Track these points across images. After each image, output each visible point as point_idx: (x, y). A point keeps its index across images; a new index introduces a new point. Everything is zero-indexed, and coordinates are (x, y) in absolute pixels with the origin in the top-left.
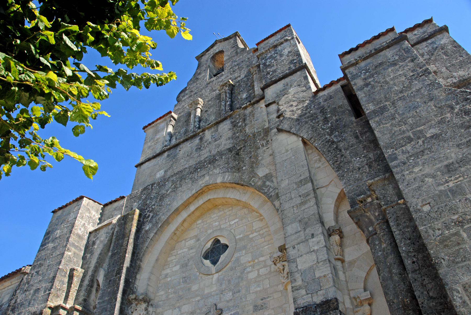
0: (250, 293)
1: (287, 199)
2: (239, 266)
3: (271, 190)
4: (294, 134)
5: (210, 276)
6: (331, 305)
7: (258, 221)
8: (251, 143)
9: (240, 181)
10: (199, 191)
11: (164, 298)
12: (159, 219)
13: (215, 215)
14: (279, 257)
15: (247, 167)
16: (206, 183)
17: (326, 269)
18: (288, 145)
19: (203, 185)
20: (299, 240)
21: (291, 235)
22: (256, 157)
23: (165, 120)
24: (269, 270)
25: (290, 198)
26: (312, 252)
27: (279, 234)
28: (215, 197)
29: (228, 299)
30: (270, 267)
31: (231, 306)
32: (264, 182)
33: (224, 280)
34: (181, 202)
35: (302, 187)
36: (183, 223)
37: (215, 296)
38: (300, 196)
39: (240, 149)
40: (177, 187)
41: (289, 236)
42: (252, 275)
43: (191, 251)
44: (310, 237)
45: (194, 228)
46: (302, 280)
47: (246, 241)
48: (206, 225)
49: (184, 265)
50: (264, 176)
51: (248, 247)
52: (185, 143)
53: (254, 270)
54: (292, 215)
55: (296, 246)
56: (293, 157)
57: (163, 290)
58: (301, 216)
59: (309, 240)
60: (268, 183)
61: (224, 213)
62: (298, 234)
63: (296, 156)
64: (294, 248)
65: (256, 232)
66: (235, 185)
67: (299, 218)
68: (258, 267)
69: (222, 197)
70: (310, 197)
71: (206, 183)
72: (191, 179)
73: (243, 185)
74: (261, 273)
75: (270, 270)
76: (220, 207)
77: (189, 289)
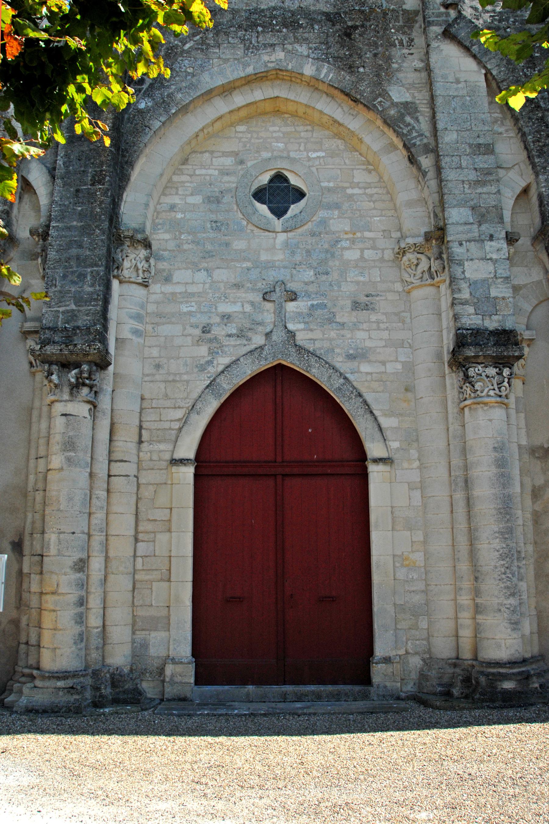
0: (346, 281)
1: (454, 165)
2: (326, 233)
3: (415, 134)
4: (474, 57)
5: (271, 234)
6: (511, 337)
7: (364, 170)
8: (377, 26)
9: (353, 91)
10: (262, 72)
11: (171, 245)
12: (169, 96)
13: (277, 128)
14: (415, 244)
15: (367, 70)
16: (277, 64)
17: (506, 290)
18: (460, 71)
19: (271, 65)
20: (470, 236)
21: (458, 224)
22: (389, 59)
24: (380, 255)
25: (459, 165)
26: (488, 259)
27: (415, 210)
28: (291, 96)
29: (306, 280)
30: (383, 252)
31: (311, 292)
32: (402, 116)
33: (298, 248)
34: (219, 81)
35: (480, 157)
36: (216, 121)
37: (282, 270)
38: (476, 169)
39: (355, 27)
40: (209, 44)
41: (453, 224)
42: (352, 255)
43: (226, 178)
44: (488, 238)
45: (230, 138)
46: (471, 294)
47: (339, 196)
48: (257, 141)
49: (212, 199)
50: (402, 104)
51: (344, 208)
53: (354, 247)
54: (461, 194)
55: (464, 243)
56: (468, 98)
57: (166, 232)
58: (475, 201)
59: (485, 242)
60: (408, 119)
61: (296, 131)
62: (469, 227)
63: (473, 98)
64: (461, 244)
65: (360, 188)
66: (336, 92)
67: (472, 203)
68: (361, 245)
69: (305, 103)
70: (491, 178)
71: (277, 64)
72: (243, 40)
73: (356, 101)
74: (366, 256)
75: (383, 257)
76: (286, 116)
77: (227, 244)
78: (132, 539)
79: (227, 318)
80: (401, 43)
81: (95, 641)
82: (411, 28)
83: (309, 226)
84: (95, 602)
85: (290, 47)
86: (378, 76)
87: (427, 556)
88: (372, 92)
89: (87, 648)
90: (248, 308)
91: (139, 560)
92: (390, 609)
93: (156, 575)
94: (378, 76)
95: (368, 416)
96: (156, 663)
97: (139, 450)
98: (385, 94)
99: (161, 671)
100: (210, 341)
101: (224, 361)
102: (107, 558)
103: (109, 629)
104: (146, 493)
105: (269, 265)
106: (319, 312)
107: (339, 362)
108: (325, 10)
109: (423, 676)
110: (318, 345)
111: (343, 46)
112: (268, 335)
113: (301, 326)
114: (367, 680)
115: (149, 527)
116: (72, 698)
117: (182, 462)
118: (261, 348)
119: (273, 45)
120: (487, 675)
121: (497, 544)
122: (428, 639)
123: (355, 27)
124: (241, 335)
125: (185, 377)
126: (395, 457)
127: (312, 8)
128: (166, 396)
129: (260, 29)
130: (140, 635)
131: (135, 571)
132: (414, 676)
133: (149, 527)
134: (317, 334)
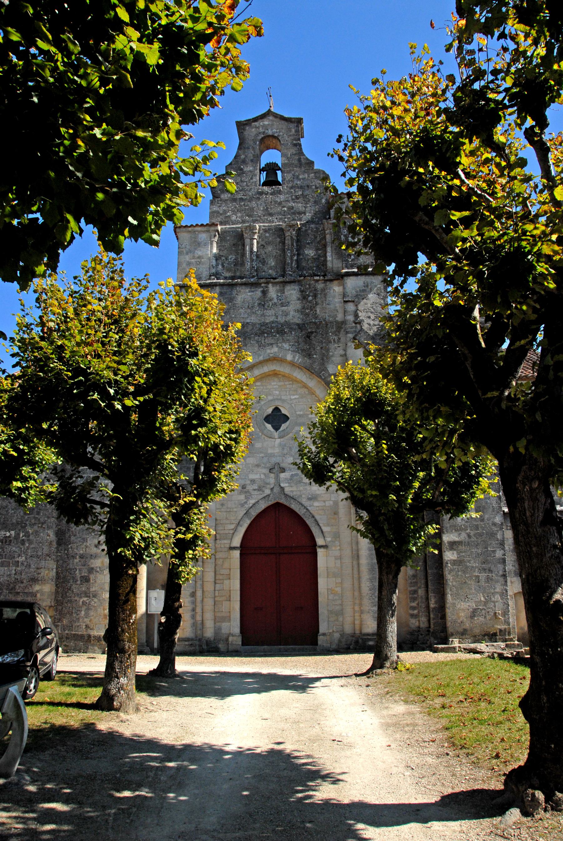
13: (275, 383)
19: (271, 355)
22: (328, 350)
23: (208, 231)
52: (244, 287)
72: (258, 342)
78: (213, 583)
79: (253, 481)
80: (334, 341)
81: (199, 626)
82: (339, 332)
83: (291, 435)
84: (199, 610)
85: (280, 345)
86: (323, 359)
87: (342, 589)
88: (320, 368)
89: (196, 629)
90: (263, 476)
91: (217, 592)
92: (326, 612)
93: (224, 598)
94: (323, 359)
95: (317, 526)
96: (225, 636)
97: (215, 543)
98: (325, 370)
99: (227, 639)
100: (246, 492)
101: (252, 502)
102: (203, 591)
103: (204, 622)
104: (219, 562)
105: (272, 455)
106: (295, 478)
107: (304, 501)
108: (298, 322)
109: (340, 641)
110: (295, 493)
111: (306, 343)
112: (272, 489)
113: (287, 485)
114: (317, 644)
115: (221, 577)
116: (192, 648)
117: (234, 548)
118: (269, 495)
119: (272, 344)
120: (362, 639)
121: (368, 584)
122: (342, 625)
123: (312, 332)
124: (260, 489)
125: (235, 510)
126: (329, 545)
127: (291, 321)
128: (227, 519)
129: (266, 335)
130: (218, 624)
131: (215, 597)
132: (336, 642)
133: (221, 577)
134: (294, 489)
